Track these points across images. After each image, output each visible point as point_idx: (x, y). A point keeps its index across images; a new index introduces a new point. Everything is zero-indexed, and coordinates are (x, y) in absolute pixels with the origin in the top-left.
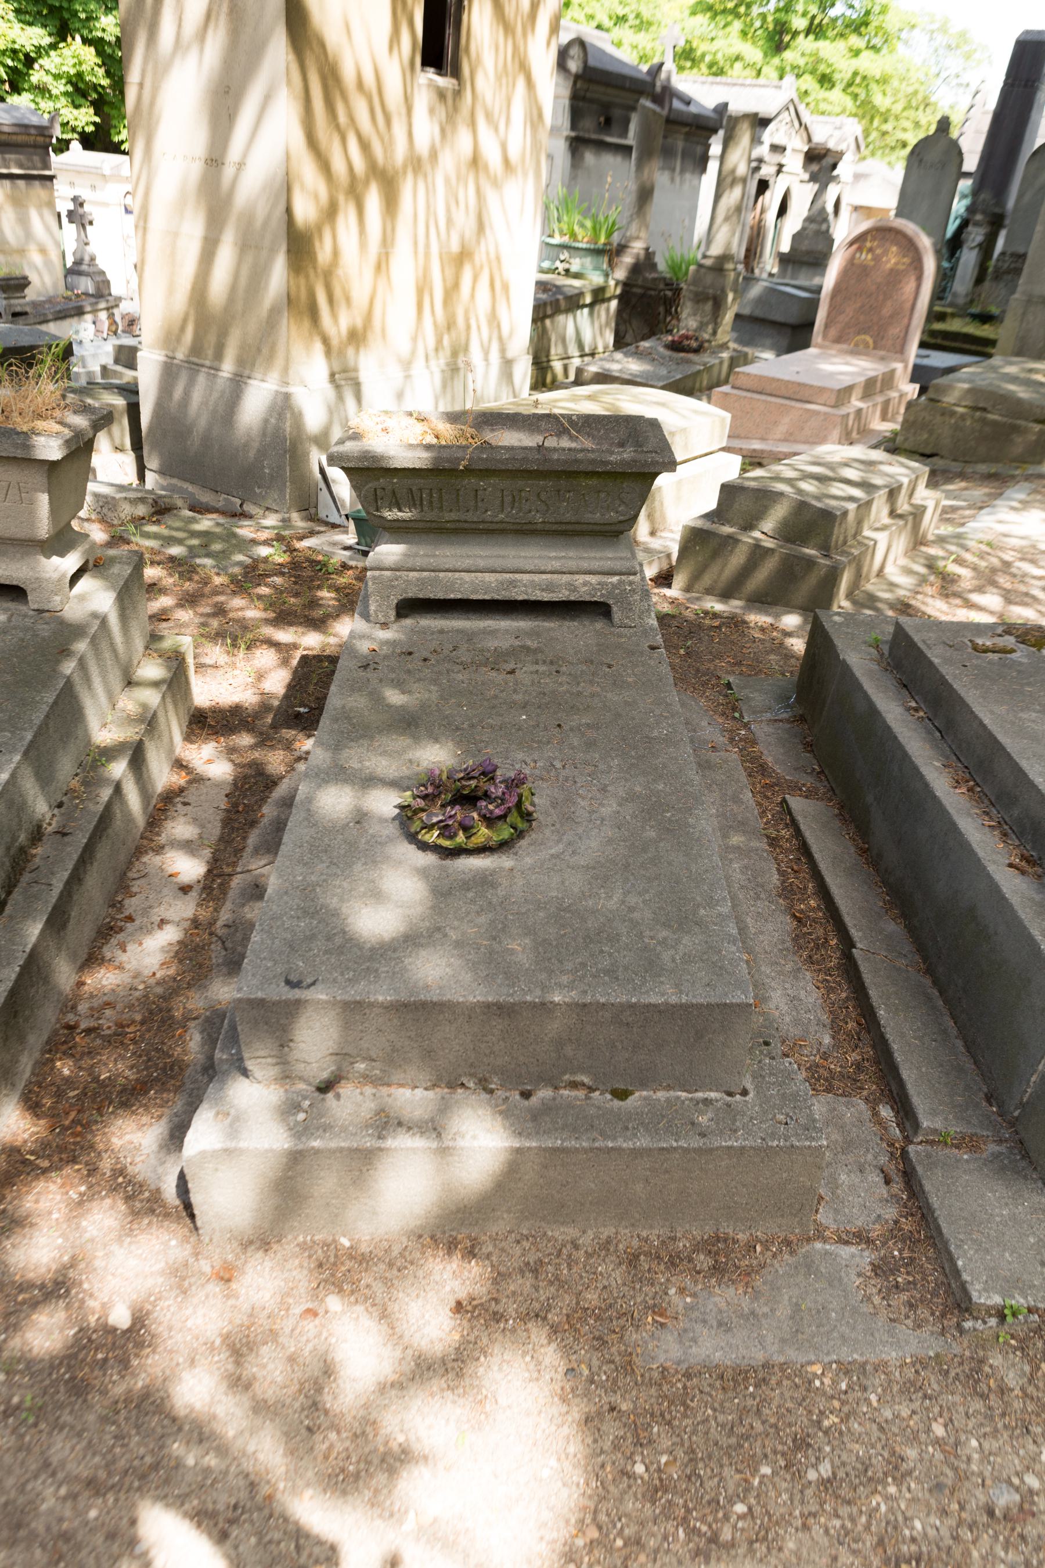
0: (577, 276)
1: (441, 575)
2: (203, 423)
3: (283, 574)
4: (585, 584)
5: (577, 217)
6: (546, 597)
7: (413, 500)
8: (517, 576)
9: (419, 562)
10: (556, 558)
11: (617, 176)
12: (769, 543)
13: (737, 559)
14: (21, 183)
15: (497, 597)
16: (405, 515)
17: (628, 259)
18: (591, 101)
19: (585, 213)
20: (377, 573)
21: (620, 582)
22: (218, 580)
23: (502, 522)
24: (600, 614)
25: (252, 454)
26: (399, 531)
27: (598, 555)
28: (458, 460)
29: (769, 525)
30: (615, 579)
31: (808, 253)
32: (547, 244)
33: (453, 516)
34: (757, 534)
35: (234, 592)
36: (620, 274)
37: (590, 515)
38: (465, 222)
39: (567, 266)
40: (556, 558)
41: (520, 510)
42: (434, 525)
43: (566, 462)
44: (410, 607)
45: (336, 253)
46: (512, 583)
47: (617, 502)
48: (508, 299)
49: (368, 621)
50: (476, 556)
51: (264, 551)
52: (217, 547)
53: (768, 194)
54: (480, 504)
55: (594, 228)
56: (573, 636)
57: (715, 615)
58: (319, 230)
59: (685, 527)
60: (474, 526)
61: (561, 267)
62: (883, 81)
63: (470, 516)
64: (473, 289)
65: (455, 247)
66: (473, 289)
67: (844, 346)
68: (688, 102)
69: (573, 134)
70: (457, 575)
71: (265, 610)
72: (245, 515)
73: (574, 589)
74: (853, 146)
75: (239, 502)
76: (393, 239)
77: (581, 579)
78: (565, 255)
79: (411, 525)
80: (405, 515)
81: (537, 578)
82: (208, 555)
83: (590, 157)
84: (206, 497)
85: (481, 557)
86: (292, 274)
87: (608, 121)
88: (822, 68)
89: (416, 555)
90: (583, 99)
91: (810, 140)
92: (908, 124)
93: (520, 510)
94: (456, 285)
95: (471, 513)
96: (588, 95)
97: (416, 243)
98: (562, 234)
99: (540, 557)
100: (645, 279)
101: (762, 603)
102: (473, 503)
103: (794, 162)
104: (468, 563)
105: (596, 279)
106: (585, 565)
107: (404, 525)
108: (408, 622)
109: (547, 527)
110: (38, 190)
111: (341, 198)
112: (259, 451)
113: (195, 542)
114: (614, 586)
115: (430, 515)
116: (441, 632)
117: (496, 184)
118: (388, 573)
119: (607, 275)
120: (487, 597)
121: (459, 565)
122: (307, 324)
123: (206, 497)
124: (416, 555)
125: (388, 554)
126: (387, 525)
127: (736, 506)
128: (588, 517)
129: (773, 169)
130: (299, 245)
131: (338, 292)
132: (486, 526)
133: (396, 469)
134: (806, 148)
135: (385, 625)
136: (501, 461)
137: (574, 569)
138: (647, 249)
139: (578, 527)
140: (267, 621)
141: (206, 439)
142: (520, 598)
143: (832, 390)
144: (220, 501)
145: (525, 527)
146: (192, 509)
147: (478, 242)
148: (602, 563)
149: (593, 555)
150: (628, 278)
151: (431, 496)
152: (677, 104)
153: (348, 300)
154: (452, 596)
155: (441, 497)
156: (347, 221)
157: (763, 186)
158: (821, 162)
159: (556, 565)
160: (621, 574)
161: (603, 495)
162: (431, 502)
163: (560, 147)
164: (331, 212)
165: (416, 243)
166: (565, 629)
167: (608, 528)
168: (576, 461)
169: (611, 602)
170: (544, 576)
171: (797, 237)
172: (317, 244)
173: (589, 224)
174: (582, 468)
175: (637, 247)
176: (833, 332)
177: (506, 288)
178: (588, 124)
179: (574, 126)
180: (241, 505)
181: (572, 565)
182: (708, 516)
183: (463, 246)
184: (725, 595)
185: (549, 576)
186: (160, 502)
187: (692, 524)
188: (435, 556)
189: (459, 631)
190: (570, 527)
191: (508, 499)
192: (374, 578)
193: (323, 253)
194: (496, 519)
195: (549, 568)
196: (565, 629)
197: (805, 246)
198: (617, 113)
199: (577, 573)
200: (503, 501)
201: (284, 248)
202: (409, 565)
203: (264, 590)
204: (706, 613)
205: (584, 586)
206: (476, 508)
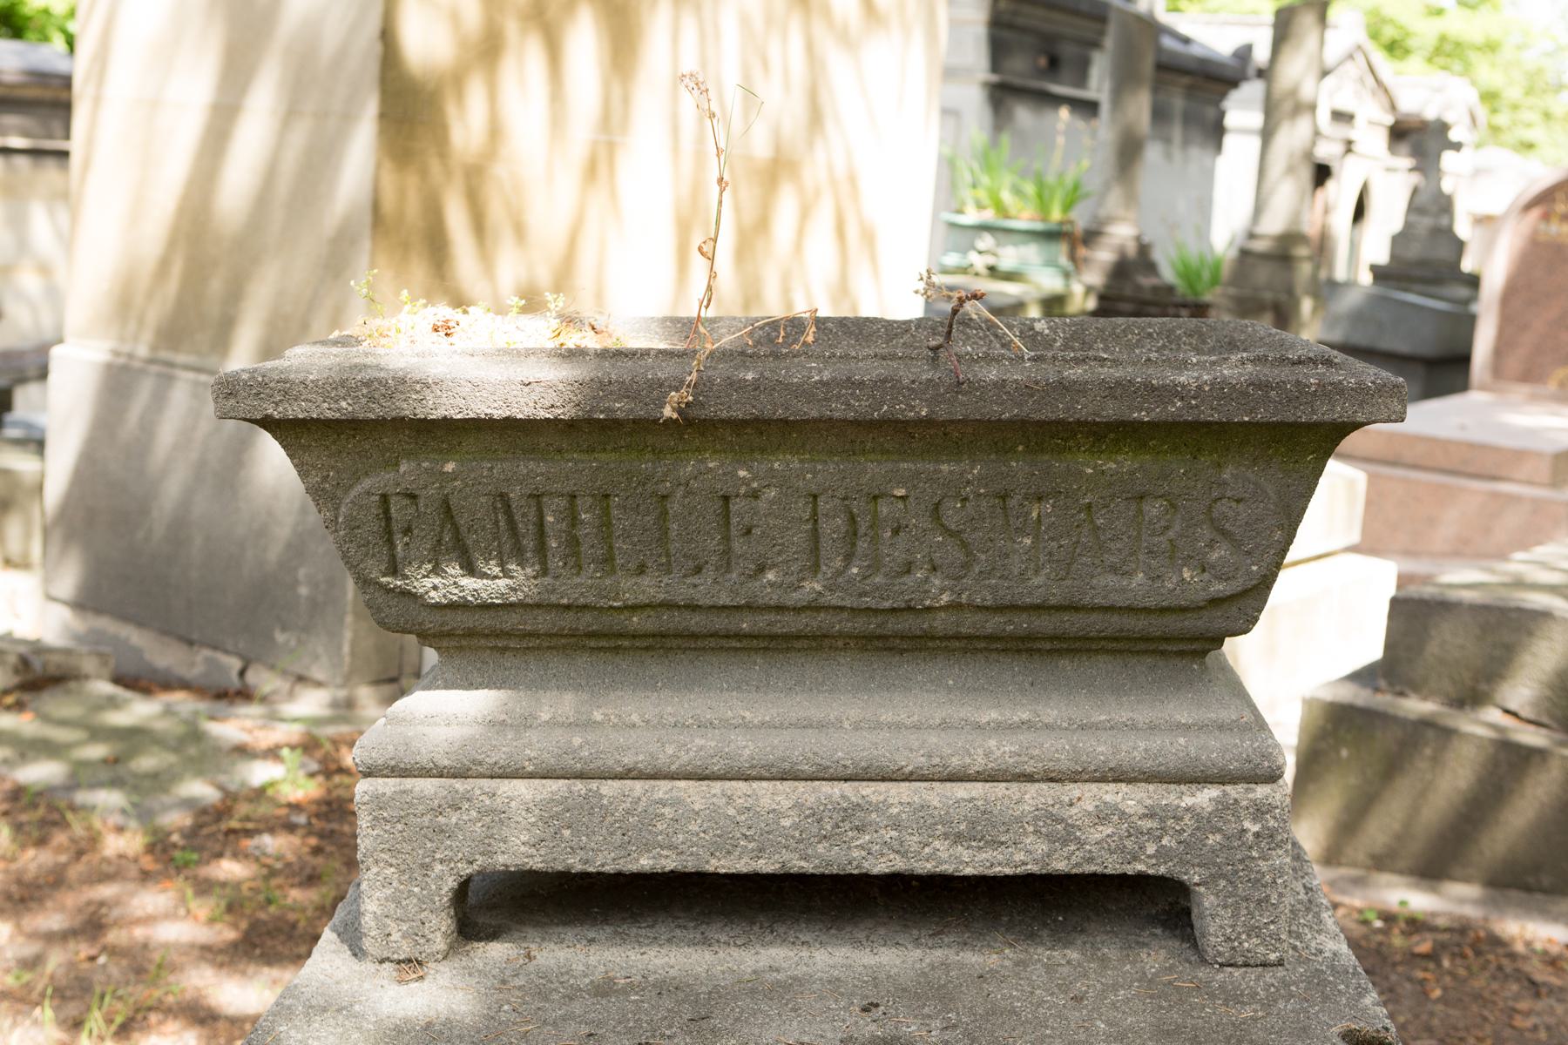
0: (1010, 277)
1: (609, 788)
2: (172, 489)
3: (291, 828)
4: (1102, 816)
5: (1007, 179)
6: (969, 861)
7: (515, 537)
8: (869, 790)
9: (536, 747)
10: (1000, 728)
11: (1069, 144)
12: (1532, 737)
13: (1455, 777)
14: (22, 162)
15: (798, 865)
16: (491, 585)
17: (1104, 255)
18: (1023, 30)
19: (1023, 174)
20: (387, 786)
21: (1225, 807)
22: (113, 845)
23: (813, 607)
24: (1153, 920)
25: (274, 553)
26: (476, 642)
27: (1143, 714)
28: (660, 388)
29: (1522, 690)
30: (1205, 797)
31: (1422, 263)
32: (953, 225)
33: (649, 588)
34: (1493, 715)
35: (145, 877)
36: (1095, 277)
37: (1111, 580)
38: (782, 103)
39: (991, 260)
40: (1000, 728)
41: (875, 566)
42: (587, 621)
43: (1027, 390)
44: (496, 905)
45: (495, 131)
46: (853, 817)
47: (1206, 532)
48: (873, 259)
49: (358, 953)
50: (726, 725)
51: (259, 773)
52: (146, 762)
53: (1331, 185)
54: (738, 546)
55: (1040, 196)
56: (1073, 1009)
57: (1416, 925)
58: (457, 80)
59: (1309, 703)
60: (720, 623)
61: (979, 262)
62: (1491, 47)
63: (704, 589)
64: (801, 232)
65: (761, 147)
66: (801, 232)
67: (1539, 389)
68: (1186, 41)
69: (994, 78)
70: (663, 788)
71: (212, 921)
72: (244, 695)
73: (1067, 835)
74: (1467, 120)
75: (235, 664)
76: (626, 117)
77: (1089, 796)
78: (986, 242)
79: (511, 621)
80: (491, 585)
81: (936, 795)
82: (115, 783)
83: (1024, 115)
84: (164, 656)
85: (746, 726)
86: (388, 164)
87: (1054, 63)
88: (1389, 33)
89: (526, 723)
90: (1010, 26)
91: (1393, 107)
92: (1534, 117)
93: (875, 566)
94: (763, 224)
95: (709, 575)
96: (1020, 21)
97: (675, 130)
98: (980, 206)
99: (944, 726)
100: (1139, 288)
101: (1528, 889)
102: (714, 543)
103: (1371, 137)
104: (699, 747)
105: (1051, 282)
106: (1100, 750)
107: (486, 621)
108: (496, 952)
109: (969, 623)
110: (50, 172)
111: (511, 28)
112: (289, 546)
113: (97, 751)
114: (1205, 823)
115: (579, 586)
116: (604, 989)
117: (846, 40)
118: (427, 786)
119: (1067, 275)
120: (766, 866)
121: (670, 753)
122: (419, 271)
123: (164, 656)
124: (526, 723)
125: (430, 719)
126: (431, 622)
127: (1433, 648)
128: (1106, 586)
129: (1338, 148)
130: (409, 109)
131: (496, 212)
132: (761, 622)
133: (447, 424)
134: (1389, 120)
135: (411, 965)
136: (804, 392)
137: (1065, 763)
138: (1138, 238)
139: (1072, 623)
140: (208, 953)
141: (180, 526)
142: (880, 867)
143: (1538, 455)
144: (192, 664)
145: (894, 625)
146: (118, 680)
147: (810, 144)
148: (1156, 742)
149: (1124, 715)
150: (1108, 287)
151: (574, 521)
152: (1168, 42)
153: (520, 231)
154: (645, 863)
155: (605, 523)
156: (524, 65)
157: (1322, 173)
158: (1416, 138)
159: (1003, 750)
160: (1223, 778)
161: (1154, 509)
162: (573, 543)
163: (972, 98)
164: (488, 50)
165: (675, 130)
166: (1037, 973)
167: (1173, 624)
168: (1063, 387)
169: (1193, 876)
170: (961, 791)
171: (1398, 241)
172: (451, 110)
173: (1030, 188)
174: (1083, 409)
175: (1122, 233)
176: (1513, 363)
177: (869, 238)
178: (1020, 66)
179: (995, 66)
180: (242, 673)
181: (1057, 749)
182: (1363, 677)
183: (778, 148)
184: (1430, 871)
185: (977, 789)
186: (37, 663)
187: (1328, 695)
188: (588, 725)
189: (664, 988)
190: (1044, 624)
191: (832, 527)
192: (378, 801)
193: (467, 126)
194: (794, 598)
195: (979, 763)
196: (1037, 973)
197: (1414, 251)
198: (1068, 51)
199: (1075, 777)
200: (815, 535)
201: (371, 108)
202: (498, 757)
203: (229, 869)
204: (1389, 918)
205: (1099, 826)
206: (727, 559)
